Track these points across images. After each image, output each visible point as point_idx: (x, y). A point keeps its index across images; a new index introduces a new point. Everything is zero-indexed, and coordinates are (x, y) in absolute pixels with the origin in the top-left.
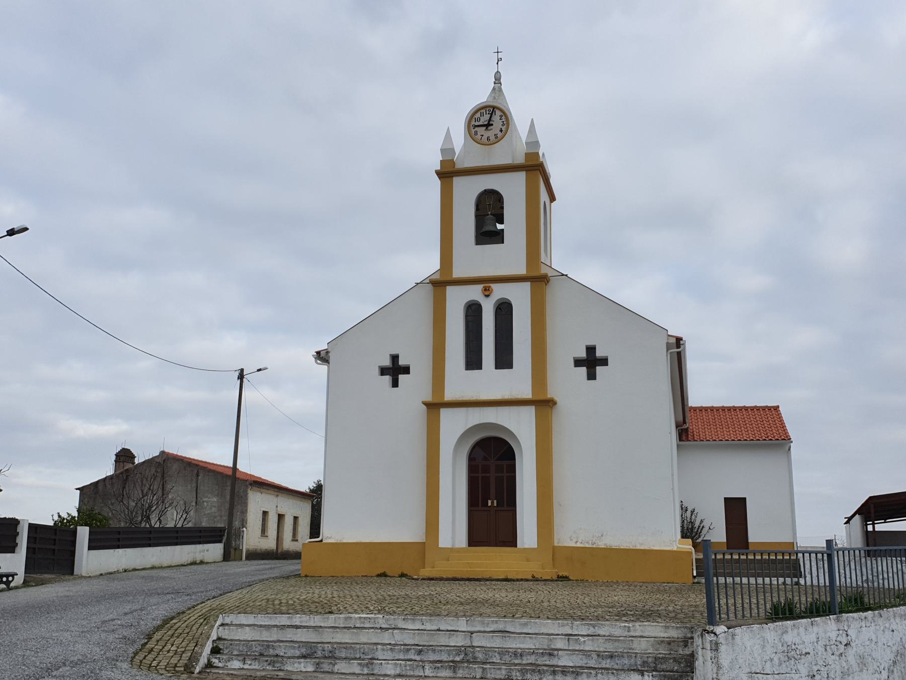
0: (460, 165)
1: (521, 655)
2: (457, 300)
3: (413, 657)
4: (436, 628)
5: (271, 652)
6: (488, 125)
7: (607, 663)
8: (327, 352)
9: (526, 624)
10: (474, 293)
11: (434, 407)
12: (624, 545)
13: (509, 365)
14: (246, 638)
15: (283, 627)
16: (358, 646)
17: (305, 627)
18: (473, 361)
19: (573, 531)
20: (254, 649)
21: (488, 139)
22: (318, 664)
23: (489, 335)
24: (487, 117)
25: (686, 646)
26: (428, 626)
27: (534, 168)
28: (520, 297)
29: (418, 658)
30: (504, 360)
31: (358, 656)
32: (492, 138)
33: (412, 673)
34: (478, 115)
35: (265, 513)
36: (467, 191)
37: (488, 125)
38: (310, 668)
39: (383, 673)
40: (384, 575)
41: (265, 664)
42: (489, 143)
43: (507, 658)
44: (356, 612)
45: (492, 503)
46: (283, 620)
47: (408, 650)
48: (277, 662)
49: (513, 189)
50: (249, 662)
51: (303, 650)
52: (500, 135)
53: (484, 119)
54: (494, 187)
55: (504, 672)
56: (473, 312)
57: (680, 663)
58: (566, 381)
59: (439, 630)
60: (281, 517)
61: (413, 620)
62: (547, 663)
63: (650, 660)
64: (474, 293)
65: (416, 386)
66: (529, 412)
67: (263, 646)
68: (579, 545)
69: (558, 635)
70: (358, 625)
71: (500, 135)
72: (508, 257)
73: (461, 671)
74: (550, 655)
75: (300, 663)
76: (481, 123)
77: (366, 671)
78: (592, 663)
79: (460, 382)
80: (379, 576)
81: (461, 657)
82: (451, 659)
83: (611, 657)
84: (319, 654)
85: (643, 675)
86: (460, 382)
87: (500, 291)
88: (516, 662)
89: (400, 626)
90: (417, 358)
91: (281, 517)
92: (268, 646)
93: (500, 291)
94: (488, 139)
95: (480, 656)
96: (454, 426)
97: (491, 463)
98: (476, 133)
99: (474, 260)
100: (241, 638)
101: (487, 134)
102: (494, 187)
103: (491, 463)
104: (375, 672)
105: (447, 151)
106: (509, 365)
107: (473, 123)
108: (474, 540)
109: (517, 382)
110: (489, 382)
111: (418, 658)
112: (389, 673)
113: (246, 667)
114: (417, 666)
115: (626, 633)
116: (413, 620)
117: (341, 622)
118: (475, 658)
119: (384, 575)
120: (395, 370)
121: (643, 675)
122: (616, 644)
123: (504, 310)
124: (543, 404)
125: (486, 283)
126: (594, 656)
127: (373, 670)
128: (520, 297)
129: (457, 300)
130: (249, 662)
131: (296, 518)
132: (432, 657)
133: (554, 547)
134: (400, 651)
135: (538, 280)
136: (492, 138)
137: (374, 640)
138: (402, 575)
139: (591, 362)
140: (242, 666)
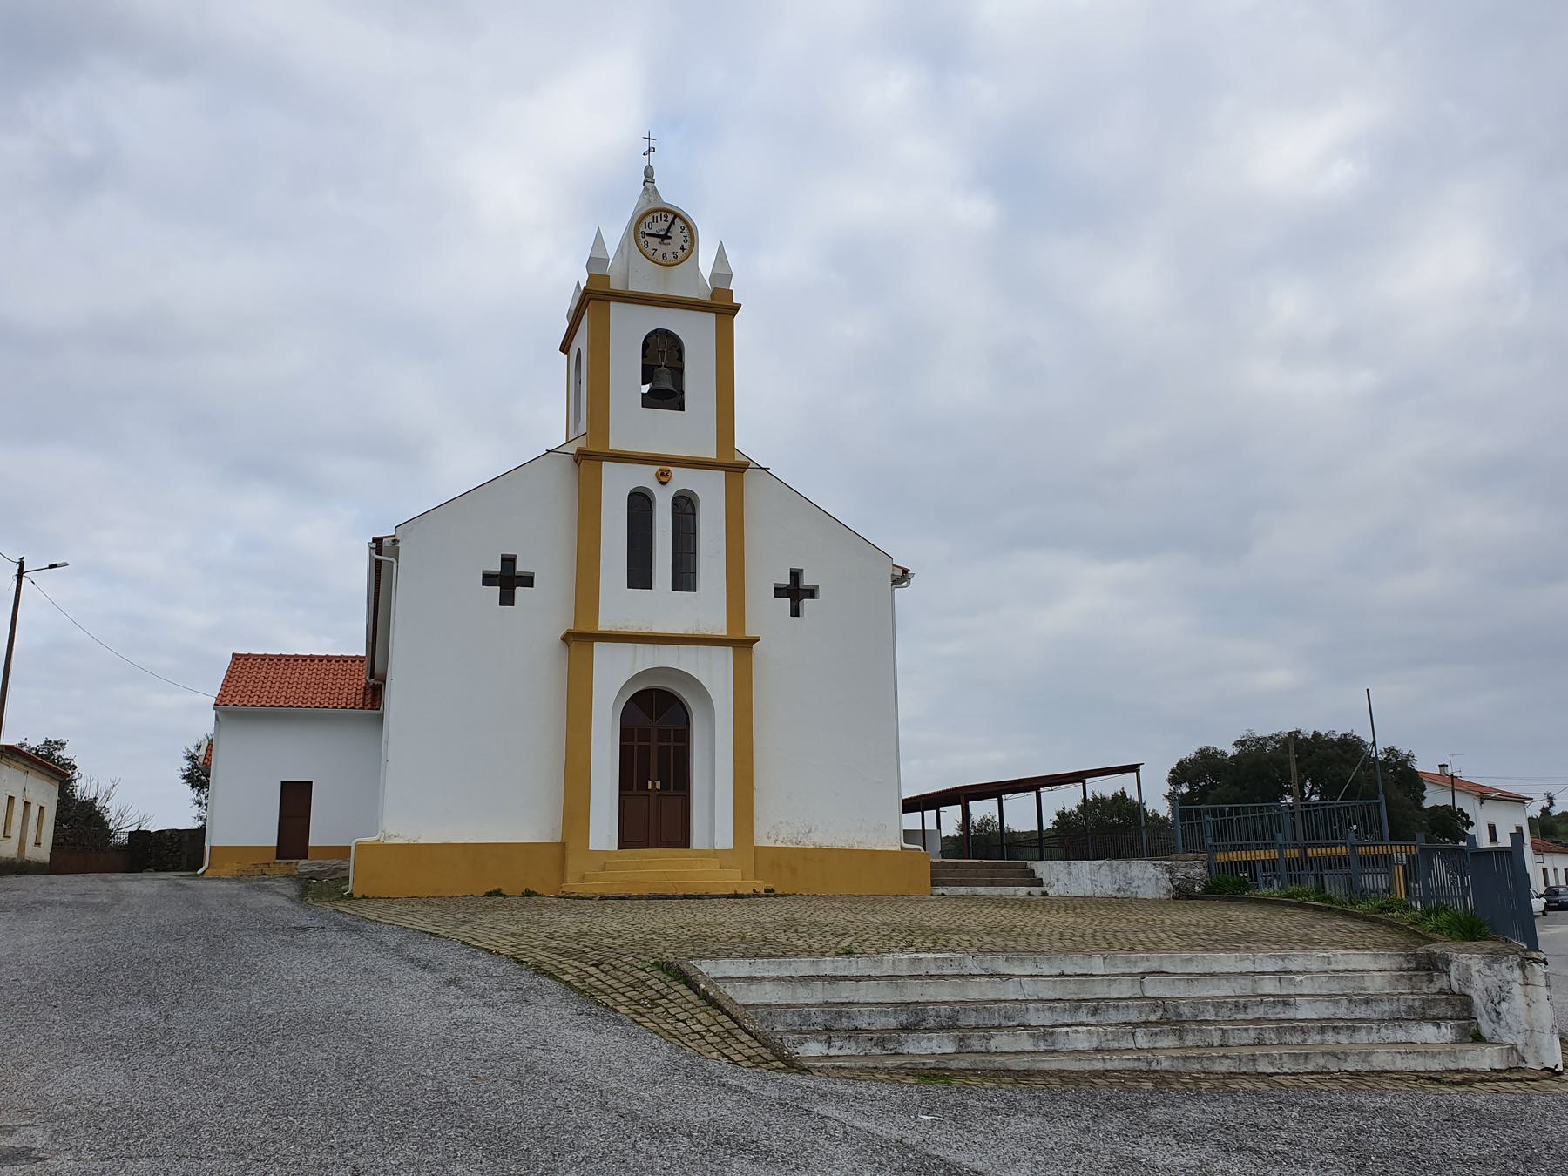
0: (616, 285)
1: (1245, 1007)
2: (617, 483)
3: (1085, 1019)
4: (1057, 972)
5: (846, 1023)
6: (664, 237)
7: (1361, 1012)
8: (396, 542)
9: (1190, 960)
10: (644, 477)
11: (581, 640)
12: (839, 845)
13: (691, 587)
14: (766, 1001)
15: (807, 979)
16: (996, 1006)
17: (846, 978)
18: (640, 575)
19: (776, 828)
20: (814, 1020)
21: (664, 256)
22: (962, 1040)
23: (662, 540)
24: (665, 226)
25: (1431, 981)
26: (1046, 970)
27: (722, 308)
28: (709, 490)
29: (1092, 1020)
30: (684, 578)
31: (996, 1023)
32: (670, 256)
33: (1116, 1045)
34: (649, 219)
35: (11, 798)
36: (629, 330)
37: (664, 237)
38: (950, 1048)
39: (1071, 1047)
40: (497, 893)
41: (869, 1045)
42: (664, 262)
43: (1225, 1013)
44: (928, 950)
45: (654, 785)
46: (828, 966)
47: (1077, 1009)
48: (890, 1040)
49: (695, 333)
50: (839, 1044)
51: (903, 1018)
52: (680, 254)
53: (659, 227)
54: (650, 321)
55: (1253, 1034)
56: (640, 504)
57: (1454, 1006)
58: (766, 615)
59: (1062, 975)
60: (27, 804)
61: (1022, 960)
62: (1281, 1016)
63: (1417, 1003)
64: (644, 477)
65: (544, 609)
66: (725, 655)
67: (829, 1013)
68: (779, 844)
69: (1263, 973)
70: (932, 972)
71: (680, 254)
72: (684, 431)
73: (1190, 1037)
74: (1286, 1004)
75: (930, 1040)
76: (653, 231)
77: (1042, 1047)
78: (1342, 1012)
79: (620, 606)
80: (489, 894)
81: (1159, 1014)
82: (1143, 1018)
83: (1367, 1002)
84: (931, 1022)
85: (1439, 1026)
86: (620, 606)
87: (682, 479)
88: (1238, 1017)
89: (1002, 971)
90: (551, 560)
91: (27, 804)
92: (839, 1013)
93: (682, 479)
94: (664, 256)
95: (1186, 1011)
96: (615, 673)
97: (657, 731)
98: (646, 244)
99: (635, 425)
100: (757, 1002)
101: (662, 249)
102: (650, 321)
103: (657, 731)
104: (1058, 1047)
105: (596, 263)
106: (691, 587)
107: (642, 229)
108: (623, 843)
109: (702, 611)
110: (661, 608)
111: (1092, 1020)
112: (1080, 1047)
113: (833, 1052)
114: (1124, 1033)
115: (1326, 967)
116: (1022, 960)
117: (905, 967)
118: (1179, 1015)
119: (497, 893)
120: (508, 580)
121: (1439, 1026)
122: (1344, 983)
123: (685, 507)
124: (742, 645)
125: (664, 464)
126: (1345, 1002)
127: (1053, 1044)
128: (709, 490)
129: (617, 483)
130: (839, 1044)
131: (42, 808)
132: (1114, 1017)
133: (756, 848)
134: (1065, 1010)
135: (735, 469)
136: (670, 256)
137: (992, 996)
138: (528, 894)
139: (796, 592)
140: (825, 1052)
